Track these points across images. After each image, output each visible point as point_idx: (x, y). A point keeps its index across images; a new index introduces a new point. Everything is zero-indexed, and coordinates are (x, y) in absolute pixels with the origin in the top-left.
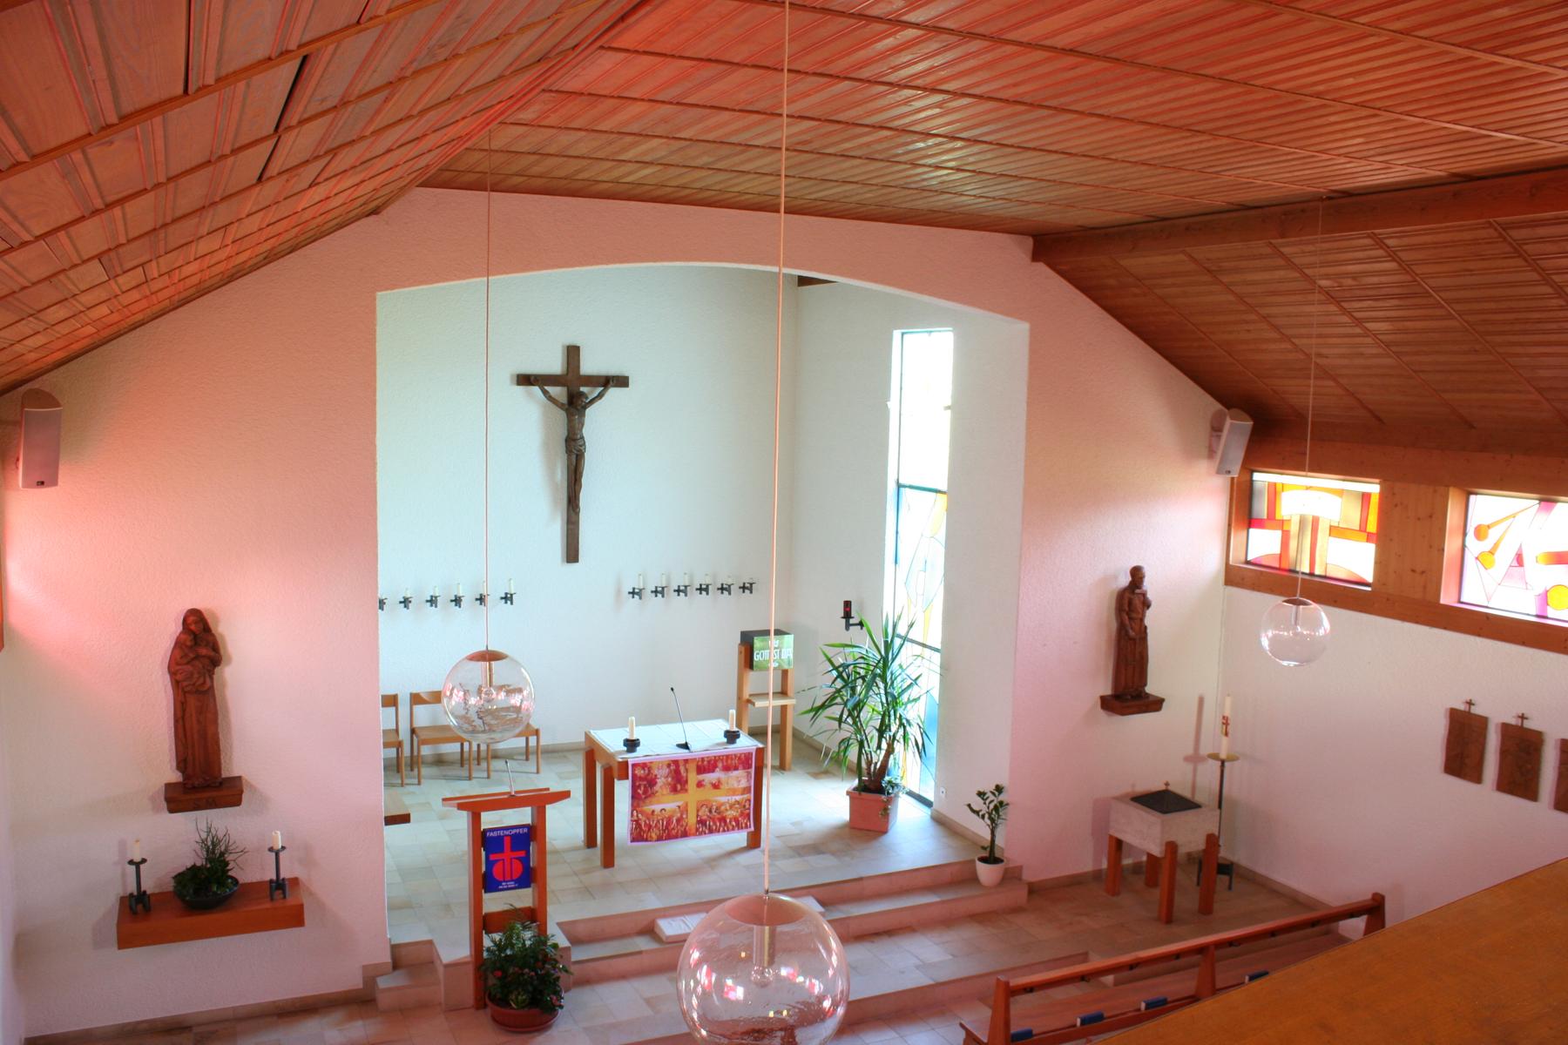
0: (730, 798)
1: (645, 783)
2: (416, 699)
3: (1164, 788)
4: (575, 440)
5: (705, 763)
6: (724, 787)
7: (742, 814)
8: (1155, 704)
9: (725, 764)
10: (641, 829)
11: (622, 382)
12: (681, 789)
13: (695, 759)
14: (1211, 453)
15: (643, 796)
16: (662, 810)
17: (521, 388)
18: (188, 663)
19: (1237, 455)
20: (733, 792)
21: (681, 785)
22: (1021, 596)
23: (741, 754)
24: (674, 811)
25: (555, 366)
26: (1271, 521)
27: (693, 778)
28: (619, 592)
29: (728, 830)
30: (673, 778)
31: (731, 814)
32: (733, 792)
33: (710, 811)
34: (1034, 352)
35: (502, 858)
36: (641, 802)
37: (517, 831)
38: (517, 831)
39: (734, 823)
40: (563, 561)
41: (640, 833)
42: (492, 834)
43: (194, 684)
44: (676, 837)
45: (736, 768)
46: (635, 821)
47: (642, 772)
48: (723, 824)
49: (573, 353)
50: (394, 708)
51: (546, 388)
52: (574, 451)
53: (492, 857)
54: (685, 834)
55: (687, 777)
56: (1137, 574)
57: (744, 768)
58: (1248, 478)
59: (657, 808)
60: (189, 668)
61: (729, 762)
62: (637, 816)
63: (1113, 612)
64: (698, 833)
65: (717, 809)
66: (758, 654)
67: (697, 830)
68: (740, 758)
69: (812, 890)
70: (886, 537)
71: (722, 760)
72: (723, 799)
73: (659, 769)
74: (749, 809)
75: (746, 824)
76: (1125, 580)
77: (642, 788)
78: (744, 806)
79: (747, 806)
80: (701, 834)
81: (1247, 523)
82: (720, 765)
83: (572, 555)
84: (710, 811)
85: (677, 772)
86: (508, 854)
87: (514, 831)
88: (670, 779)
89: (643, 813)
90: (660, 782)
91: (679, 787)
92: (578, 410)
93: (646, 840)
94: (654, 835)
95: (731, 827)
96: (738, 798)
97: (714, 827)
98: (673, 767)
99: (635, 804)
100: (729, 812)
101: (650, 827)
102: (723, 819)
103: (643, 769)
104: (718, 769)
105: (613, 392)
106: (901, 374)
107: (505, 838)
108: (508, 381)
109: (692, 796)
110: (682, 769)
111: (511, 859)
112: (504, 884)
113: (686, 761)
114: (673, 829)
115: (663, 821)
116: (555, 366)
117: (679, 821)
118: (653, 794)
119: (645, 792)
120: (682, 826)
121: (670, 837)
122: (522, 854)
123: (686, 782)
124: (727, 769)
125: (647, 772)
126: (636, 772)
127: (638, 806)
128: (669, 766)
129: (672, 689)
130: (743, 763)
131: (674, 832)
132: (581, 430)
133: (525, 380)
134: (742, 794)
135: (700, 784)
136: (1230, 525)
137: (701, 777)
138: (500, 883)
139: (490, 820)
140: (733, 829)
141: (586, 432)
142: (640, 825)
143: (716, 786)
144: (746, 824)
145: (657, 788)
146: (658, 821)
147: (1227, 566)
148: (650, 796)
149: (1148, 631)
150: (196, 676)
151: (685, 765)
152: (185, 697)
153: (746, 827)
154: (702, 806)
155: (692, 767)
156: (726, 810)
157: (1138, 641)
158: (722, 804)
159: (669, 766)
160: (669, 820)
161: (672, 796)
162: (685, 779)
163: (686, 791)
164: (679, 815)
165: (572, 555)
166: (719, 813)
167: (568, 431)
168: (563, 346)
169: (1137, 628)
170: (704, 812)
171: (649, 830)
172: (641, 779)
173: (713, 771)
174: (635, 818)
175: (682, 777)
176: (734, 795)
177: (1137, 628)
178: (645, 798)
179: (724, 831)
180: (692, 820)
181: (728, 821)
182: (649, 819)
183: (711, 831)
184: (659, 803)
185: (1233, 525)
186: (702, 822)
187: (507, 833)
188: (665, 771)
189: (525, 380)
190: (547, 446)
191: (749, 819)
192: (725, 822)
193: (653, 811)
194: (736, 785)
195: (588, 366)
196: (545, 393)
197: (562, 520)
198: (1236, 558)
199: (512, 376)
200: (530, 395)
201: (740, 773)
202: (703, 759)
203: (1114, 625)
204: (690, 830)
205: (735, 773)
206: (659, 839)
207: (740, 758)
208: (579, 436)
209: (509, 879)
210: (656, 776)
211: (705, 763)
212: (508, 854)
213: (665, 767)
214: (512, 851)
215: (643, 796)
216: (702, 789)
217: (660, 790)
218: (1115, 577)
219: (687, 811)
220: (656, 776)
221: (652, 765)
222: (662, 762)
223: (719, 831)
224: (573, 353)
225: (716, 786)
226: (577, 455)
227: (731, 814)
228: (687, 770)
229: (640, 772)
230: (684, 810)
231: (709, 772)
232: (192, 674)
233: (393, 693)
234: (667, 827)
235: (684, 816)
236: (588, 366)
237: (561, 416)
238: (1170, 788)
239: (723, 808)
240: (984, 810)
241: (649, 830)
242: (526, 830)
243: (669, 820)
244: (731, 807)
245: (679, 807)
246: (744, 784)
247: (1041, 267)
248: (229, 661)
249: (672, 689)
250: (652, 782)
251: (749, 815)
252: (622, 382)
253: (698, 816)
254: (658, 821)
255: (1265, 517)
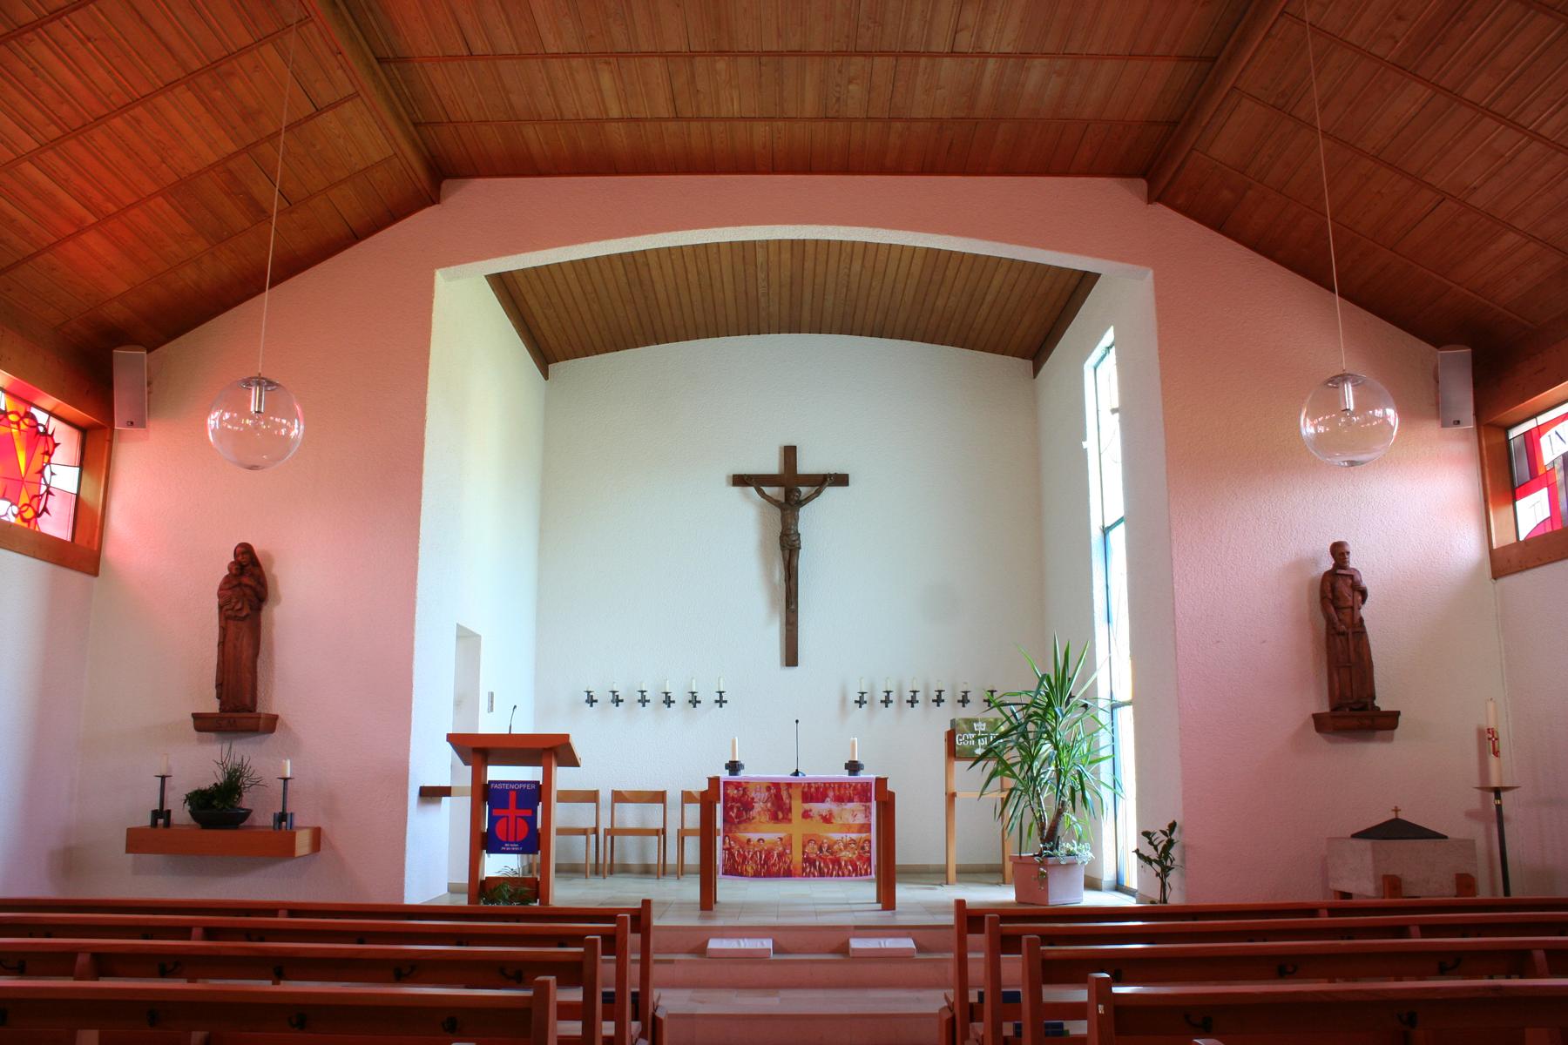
0: (844, 835)
1: (739, 805)
2: (618, 797)
3: (1392, 816)
4: (788, 535)
5: (813, 790)
6: (837, 821)
7: (860, 857)
8: (1390, 721)
9: (837, 793)
10: (734, 860)
11: (841, 480)
12: (783, 819)
13: (801, 784)
14: (1438, 417)
15: (736, 820)
16: (759, 840)
17: (737, 489)
18: (230, 589)
19: (1462, 398)
20: (848, 828)
21: (783, 813)
22: (1176, 578)
23: (857, 783)
24: (775, 844)
25: (773, 466)
26: (1537, 478)
27: (798, 806)
28: (844, 700)
29: (843, 876)
30: (773, 804)
31: (846, 855)
32: (848, 828)
33: (820, 849)
34: (1159, 299)
35: (506, 815)
36: (734, 827)
37: (524, 786)
38: (524, 786)
39: (850, 868)
40: (782, 665)
41: (733, 864)
42: (496, 786)
43: (232, 609)
44: (777, 875)
45: (851, 800)
46: (728, 849)
47: (736, 792)
48: (837, 867)
49: (790, 453)
50: (595, 804)
51: (764, 488)
52: (789, 546)
53: (496, 813)
54: (788, 874)
55: (790, 804)
56: (1339, 551)
57: (861, 801)
58: (1503, 439)
59: (754, 837)
60: (229, 593)
61: (842, 792)
62: (730, 844)
63: (1318, 606)
64: (804, 874)
65: (829, 848)
66: (960, 737)
67: (804, 870)
68: (855, 788)
69: (913, 931)
70: (1095, 598)
71: (834, 788)
72: (836, 836)
73: (756, 791)
74: (869, 852)
75: (866, 871)
76: (1328, 564)
77: (735, 810)
78: (863, 848)
79: (867, 848)
80: (808, 875)
81: (1510, 494)
82: (831, 794)
83: (791, 658)
84: (820, 849)
85: (778, 797)
86: (512, 811)
87: (520, 786)
88: (769, 805)
89: (736, 840)
90: (758, 806)
91: (780, 815)
92: (792, 506)
93: (741, 875)
94: (749, 869)
95: (847, 873)
96: (854, 836)
97: (826, 870)
98: (773, 791)
99: (727, 829)
100: (843, 853)
101: (745, 858)
102: (837, 861)
103: (737, 788)
104: (828, 799)
105: (830, 492)
106: (1098, 411)
107: (511, 793)
108: (724, 484)
109: (797, 829)
110: (784, 794)
111: (516, 817)
112: (506, 845)
113: (789, 785)
114: (774, 865)
115: (761, 852)
116: (773, 466)
117: (780, 856)
118: (749, 820)
119: (739, 815)
120: (785, 862)
121: (770, 874)
122: (529, 813)
123: (790, 810)
124: (839, 799)
125: (741, 792)
126: (729, 791)
127: (731, 831)
128: (768, 789)
129: (797, 721)
130: (858, 793)
131: (775, 869)
132: (796, 525)
133: (740, 480)
134: (860, 832)
135: (806, 815)
136: (1486, 501)
137: (807, 806)
138: (503, 844)
139: (496, 773)
140: (850, 875)
141: (802, 528)
142: (733, 855)
143: (827, 819)
144: (866, 871)
145: (753, 813)
146: (755, 853)
147: (1491, 551)
148: (745, 821)
149: (1366, 624)
150: (234, 600)
151: (787, 790)
152: (226, 623)
153: (866, 874)
154: (809, 841)
155: (797, 793)
156: (841, 850)
157: (1350, 636)
158: (836, 842)
159: (768, 789)
160: (769, 854)
161: (772, 825)
162: (788, 806)
163: (790, 821)
164: (781, 849)
165: (791, 658)
166: (832, 854)
167: (783, 527)
168: (780, 448)
169: (1348, 619)
170: (812, 849)
171: (743, 862)
172: (733, 799)
173: (823, 801)
174: (728, 846)
175: (785, 804)
176: (849, 832)
177: (1348, 619)
178: (740, 823)
179: (839, 876)
180: (797, 857)
181: (843, 864)
182: (743, 848)
183: (822, 874)
184: (756, 831)
185: (1490, 500)
186: (808, 861)
187: (513, 787)
188: (765, 795)
189: (740, 480)
190: (764, 545)
191: (870, 865)
192: (840, 865)
193: (749, 840)
194: (851, 821)
195: (806, 466)
196: (763, 494)
197: (781, 621)
198: (1502, 537)
199: (728, 477)
200: (747, 496)
201: (855, 806)
202: (809, 784)
203: (1322, 623)
204: (795, 869)
205: (850, 805)
206: (757, 875)
207: (855, 788)
208: (792, 532)
209: (513, 840)
210: (753, 799)
211: (813, 790)
212: (512, 811)
213: (764, 790)
214: (517, 808)
215: (736, 820)
216: (809, 820)
217: (758, 817)
218: (1315, 562)
219: (791, 845)
220: (753, 799)
221: (748, 786)
222: (759, 784)
223: (831, 876)
224: (790, 453)
225: (827, 819)
226: (791, 550)
227: (846, 855)
228: (790, 797)
229: (732, 792)
230: (787, 843)
231: (817, 802)
232: (231, 599)
233: (595, 789)
234: (766, 862)
235: (788, 851)
236: (806, 466)
237: (776, 513)
238: (1402, 816)
239: (836, 847)
240: (1154, 855)
241: (743, 862)
242: (533, 787)
243: (769, 854)
244: (846, 846)
245: (781, 839)
246: (860, 819)
247: (1159, 208)
248: (278, 600)
249: (797, 721)
250: (747, 805)
251: (869, 859)
252: (841, 480)
253: (804, 853)
254: (755, 853)
255: (1528, 479)
